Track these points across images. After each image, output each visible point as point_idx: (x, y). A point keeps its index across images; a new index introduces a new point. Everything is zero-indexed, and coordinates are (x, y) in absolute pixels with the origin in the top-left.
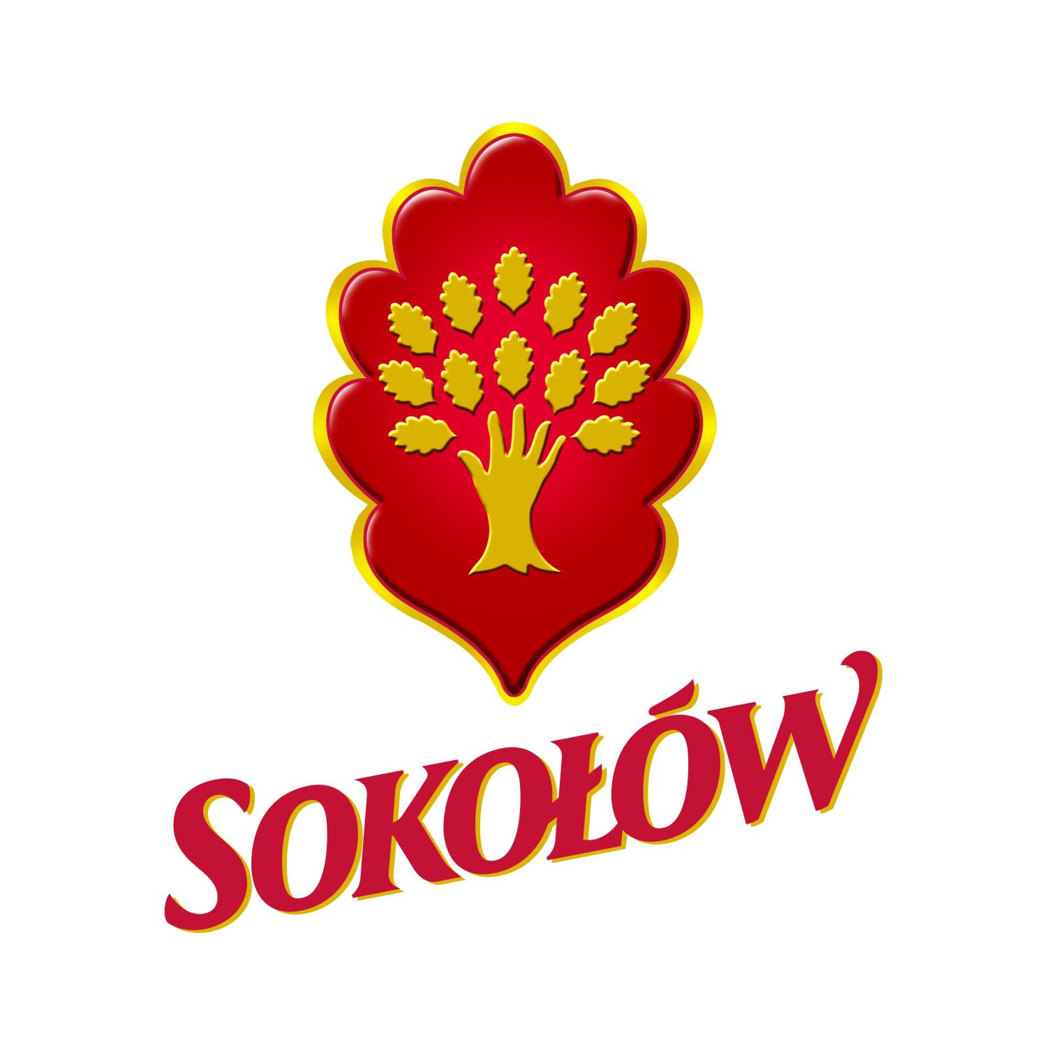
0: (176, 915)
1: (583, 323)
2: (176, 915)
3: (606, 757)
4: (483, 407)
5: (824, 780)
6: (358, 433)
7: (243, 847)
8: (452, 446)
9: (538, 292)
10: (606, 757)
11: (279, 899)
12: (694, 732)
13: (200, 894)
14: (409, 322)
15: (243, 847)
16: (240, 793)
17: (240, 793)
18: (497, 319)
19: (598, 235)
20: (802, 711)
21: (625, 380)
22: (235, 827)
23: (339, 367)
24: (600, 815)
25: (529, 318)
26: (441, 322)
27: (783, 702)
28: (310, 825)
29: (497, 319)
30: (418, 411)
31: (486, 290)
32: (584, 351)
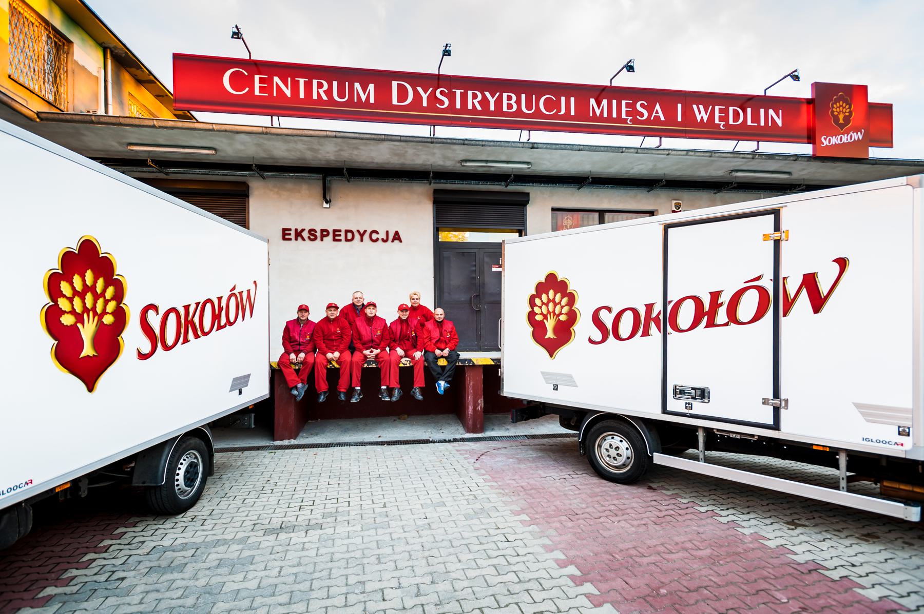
0: (591, 341)
1: (104, 291)
2: (591, 341)
3: (725, 298)
4: (83, 313)
5: (818, 302)
6: (52, 316)
7: (609, 325)
8: (76, 323)
9: (95, 282)
10: (725, 298)
11: (617, 337)
12: (762, 291)
13: (598, 336)
14: (65, 287)
15: (609, 325)
16: (609, 309)
17: (609, 309)
18: (86, 289)
19: (104, 268)
20: (810, 282)
21: (111, 306)
22: (607, 319)
23: (46, 300)
24: (722, 316)
25: (93, 289)
26: (73, 288)
27: (104, 381)
28: (628, 318)
29: (86, 289)
30: (68, 313)
31: (84, 281)
32: (105, 297)
